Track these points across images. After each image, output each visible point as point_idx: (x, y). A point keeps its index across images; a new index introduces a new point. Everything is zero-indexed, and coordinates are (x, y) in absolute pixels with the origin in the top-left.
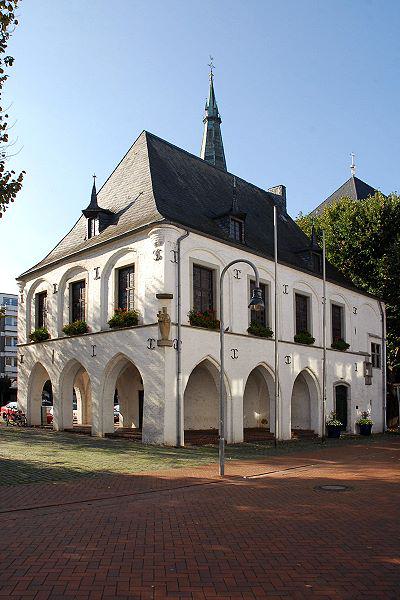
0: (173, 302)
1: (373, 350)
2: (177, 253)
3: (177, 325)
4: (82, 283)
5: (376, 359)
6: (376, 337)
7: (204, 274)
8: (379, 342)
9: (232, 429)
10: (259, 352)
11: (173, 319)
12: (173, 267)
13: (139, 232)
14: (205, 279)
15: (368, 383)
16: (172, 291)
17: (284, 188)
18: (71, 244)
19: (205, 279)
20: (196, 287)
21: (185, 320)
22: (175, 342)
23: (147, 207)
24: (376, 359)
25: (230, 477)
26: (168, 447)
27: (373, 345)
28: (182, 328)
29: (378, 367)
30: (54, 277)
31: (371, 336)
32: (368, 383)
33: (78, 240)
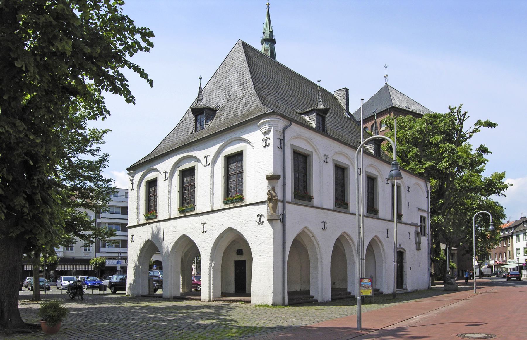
0: (280, 181)
1: (421, 222)
2: (282, 140)
3: (282, 201)
4: (192, 171)
5: (423, 229)
6: (424, 211)
7: (301, 159)
8: (425, 215)
9: (322, 289)
10: (341, 223)
11: (280, 197)
12: (280, 152)
13: (249, 122)
14: (302, 160)
15: (418, 249)
16: (280, 173)
17: (347, 90)
18: (178, 141)
19: (302, 160)
20: (296, 171)
21: (289, 196)
22: (281, 217)
23: (252, 103)
24: (423, 229)
25: (365, 329)
26: (389, 295)
27: (421, 217)
28: (287, 205)
29: (424, 235)
30: (166, 166)
31: (420, 210)
32: (418, 249)
33: (188, 133)
